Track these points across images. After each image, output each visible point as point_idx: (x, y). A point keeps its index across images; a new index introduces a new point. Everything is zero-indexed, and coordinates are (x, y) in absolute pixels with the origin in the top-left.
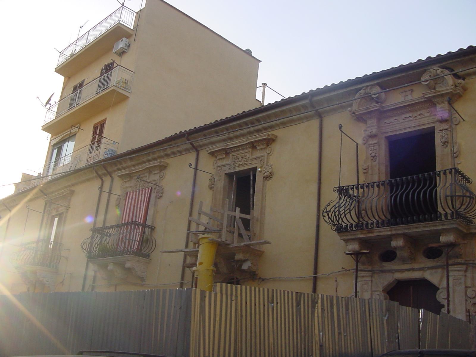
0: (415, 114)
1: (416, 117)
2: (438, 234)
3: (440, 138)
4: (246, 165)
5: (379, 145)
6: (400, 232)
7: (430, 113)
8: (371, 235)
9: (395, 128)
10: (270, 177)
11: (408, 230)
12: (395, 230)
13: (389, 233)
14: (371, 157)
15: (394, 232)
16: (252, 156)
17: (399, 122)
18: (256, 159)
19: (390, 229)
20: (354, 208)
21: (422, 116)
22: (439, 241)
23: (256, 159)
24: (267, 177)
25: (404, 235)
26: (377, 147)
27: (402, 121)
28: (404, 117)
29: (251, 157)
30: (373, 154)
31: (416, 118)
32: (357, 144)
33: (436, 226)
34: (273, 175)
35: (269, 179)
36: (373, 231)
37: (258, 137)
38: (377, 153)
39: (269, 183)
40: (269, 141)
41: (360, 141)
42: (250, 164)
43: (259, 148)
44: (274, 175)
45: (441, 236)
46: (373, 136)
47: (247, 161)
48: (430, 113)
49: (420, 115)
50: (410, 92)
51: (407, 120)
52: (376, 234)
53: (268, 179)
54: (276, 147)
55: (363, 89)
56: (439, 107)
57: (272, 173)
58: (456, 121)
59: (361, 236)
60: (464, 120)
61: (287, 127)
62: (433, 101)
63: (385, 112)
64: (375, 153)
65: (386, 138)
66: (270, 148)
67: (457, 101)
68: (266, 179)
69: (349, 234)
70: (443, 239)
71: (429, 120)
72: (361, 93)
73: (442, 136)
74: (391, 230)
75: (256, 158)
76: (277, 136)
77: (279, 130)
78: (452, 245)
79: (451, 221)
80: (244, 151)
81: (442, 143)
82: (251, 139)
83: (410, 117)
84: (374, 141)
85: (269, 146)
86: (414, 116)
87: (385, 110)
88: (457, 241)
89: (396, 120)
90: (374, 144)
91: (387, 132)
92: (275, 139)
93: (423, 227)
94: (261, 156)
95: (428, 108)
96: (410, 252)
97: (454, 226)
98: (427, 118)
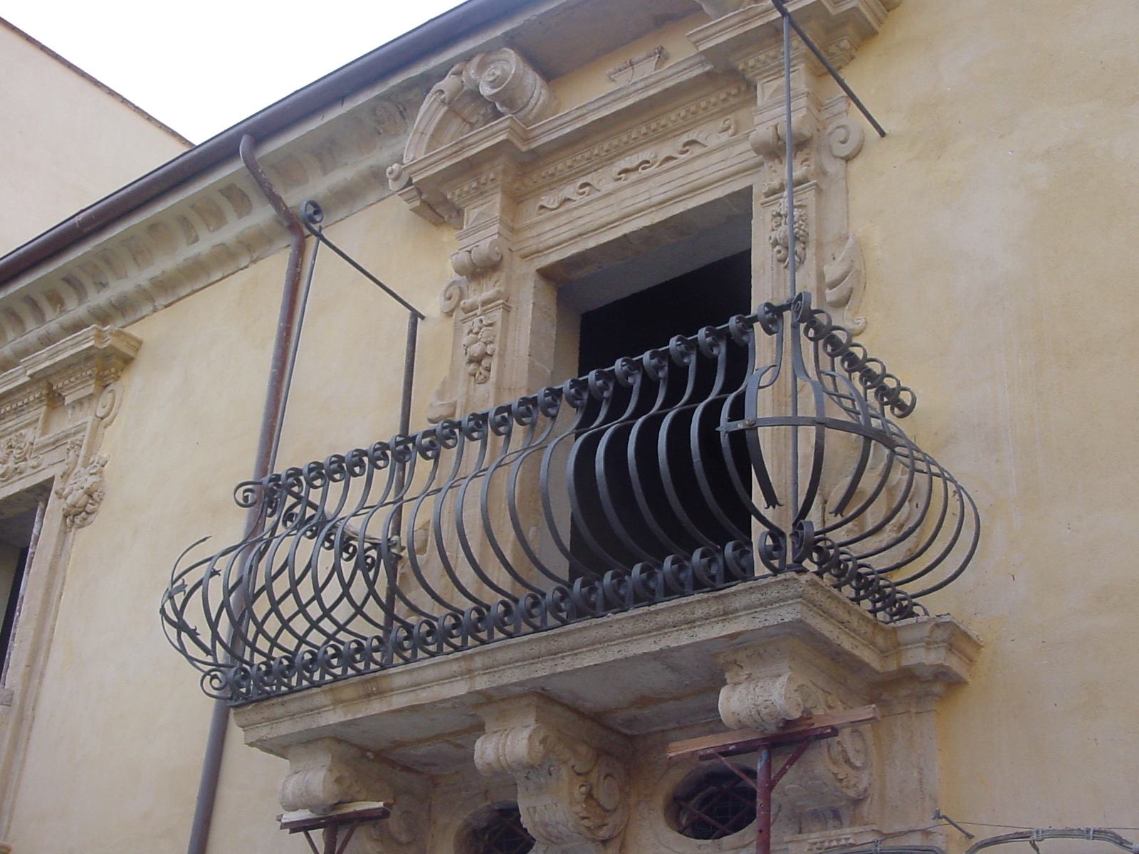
0: (667, 149)
1: (669, 158)
2: (711, 671)
3: (770, 229)
4: (20, 473)
5: (507, 309)
6: (513, 676)
7: (731, 131)
8: (377, 707)
9: (581, 222)
10: (87, 513)
11: (551, 663)
12: (487, 669)
13: (459, 688)
14: (470, 362)
15: (482, 683)
16: (43, 434)
17: (598, 194)
18: (56, 444)
19: (464, 665)
20: (309, 574)
21: (697, 150)
22: (714, 723)
23: (56, 444)
24: (74, 510)
25: (543, 697)
26: (497, 315)
27: (608, 186)
28: (619, 170)
29: (40, 440)
30: (476, 349)
31: (672, 163)
32: (416, 316)
33: (691, 623)
34: (99, 503)
35: (85, 519)
36: (384, 684)
37: (64, 350)
38: (491, 342)
39: (82, 537)
40: (109, 366)
41: (432, 307)
42: (33, 467)
43: (71, 400)
44: (103, 503)
45: (724, 683)
46: (479, 270)
47: (25, 460)
48: (731, 131)
49: (687, 148)
50: (654, 60)
51: (633, 177)
52: (398, 701)
53: (77, 520)
54: (132, 386)
55: (450, 73)
56: (767, 90)
57: (95, 495)
58: (844, 142)
59: (333, 717)
60: (883, 134)
61: (179, 299)
62: (741, 67)
63: (538, 157)
64: (486, 344)
65: (546, 274)
66: (110, 394)
67: (853, 58)
68: (73, 521)
69: (279, 711)
70: (735, 701)
71: (729, 163)
72: (442, 92)
73: (779, 215)
74: (469, 673)
75: (54, 443)
76: (140, 343)
77: (155, 314)
78: (790, 738)
79: (767, 586)
80: (21, 418)
81: (778, 248)
82: (39, 363)
83: (648, 162)
84: (488, 290)
85: (109, 388)
86: (661, 157)
87: (534, 145)
88: (819, 712)
89: (587, 189)
90: (484, 303)
91: (547, 249)
92: (131, 353)
93: (626, 636)
94: (73, 431)
95: (724, 112)
96: (589, 796)
97: (788, 614)
98: (716, 157)
